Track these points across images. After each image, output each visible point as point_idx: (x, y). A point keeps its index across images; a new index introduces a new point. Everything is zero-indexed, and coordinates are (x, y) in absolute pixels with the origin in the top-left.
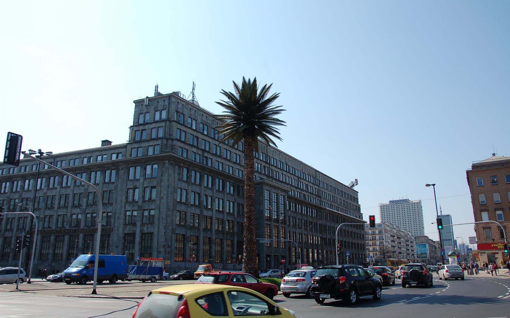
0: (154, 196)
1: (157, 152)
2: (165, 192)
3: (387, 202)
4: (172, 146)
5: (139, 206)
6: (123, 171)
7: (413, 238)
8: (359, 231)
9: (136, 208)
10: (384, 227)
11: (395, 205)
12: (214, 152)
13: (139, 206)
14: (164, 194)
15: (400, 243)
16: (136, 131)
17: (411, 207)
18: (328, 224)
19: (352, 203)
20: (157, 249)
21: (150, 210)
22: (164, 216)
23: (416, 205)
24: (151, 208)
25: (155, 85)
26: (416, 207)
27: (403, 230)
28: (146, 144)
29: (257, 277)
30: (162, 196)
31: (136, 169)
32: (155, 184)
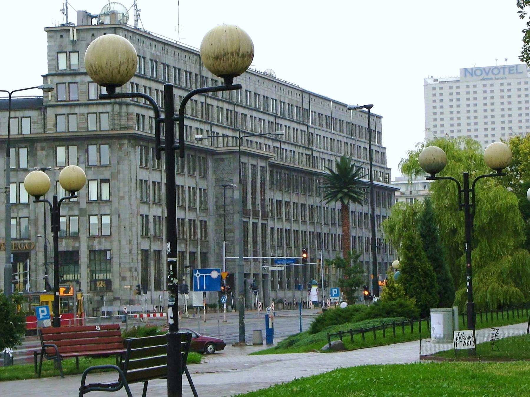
0: (105, 196)
1: (105, 125)
2: (127, 189)
3: (455, 74)
4: (128, 114)
5: (81, 210)
6: (44, 153)
8: (383, 210)
9: (77, 212)
11: (480, 84)
13: (81, 210)
14: (124, 192)
16: (57, 84)
20: (120, 273)
21: (101, 215)
22: (127, 224)
24: (102, 213)
28: (84, 110)
30: (121, 194)
31: (68, 149)
32: (106, 175)
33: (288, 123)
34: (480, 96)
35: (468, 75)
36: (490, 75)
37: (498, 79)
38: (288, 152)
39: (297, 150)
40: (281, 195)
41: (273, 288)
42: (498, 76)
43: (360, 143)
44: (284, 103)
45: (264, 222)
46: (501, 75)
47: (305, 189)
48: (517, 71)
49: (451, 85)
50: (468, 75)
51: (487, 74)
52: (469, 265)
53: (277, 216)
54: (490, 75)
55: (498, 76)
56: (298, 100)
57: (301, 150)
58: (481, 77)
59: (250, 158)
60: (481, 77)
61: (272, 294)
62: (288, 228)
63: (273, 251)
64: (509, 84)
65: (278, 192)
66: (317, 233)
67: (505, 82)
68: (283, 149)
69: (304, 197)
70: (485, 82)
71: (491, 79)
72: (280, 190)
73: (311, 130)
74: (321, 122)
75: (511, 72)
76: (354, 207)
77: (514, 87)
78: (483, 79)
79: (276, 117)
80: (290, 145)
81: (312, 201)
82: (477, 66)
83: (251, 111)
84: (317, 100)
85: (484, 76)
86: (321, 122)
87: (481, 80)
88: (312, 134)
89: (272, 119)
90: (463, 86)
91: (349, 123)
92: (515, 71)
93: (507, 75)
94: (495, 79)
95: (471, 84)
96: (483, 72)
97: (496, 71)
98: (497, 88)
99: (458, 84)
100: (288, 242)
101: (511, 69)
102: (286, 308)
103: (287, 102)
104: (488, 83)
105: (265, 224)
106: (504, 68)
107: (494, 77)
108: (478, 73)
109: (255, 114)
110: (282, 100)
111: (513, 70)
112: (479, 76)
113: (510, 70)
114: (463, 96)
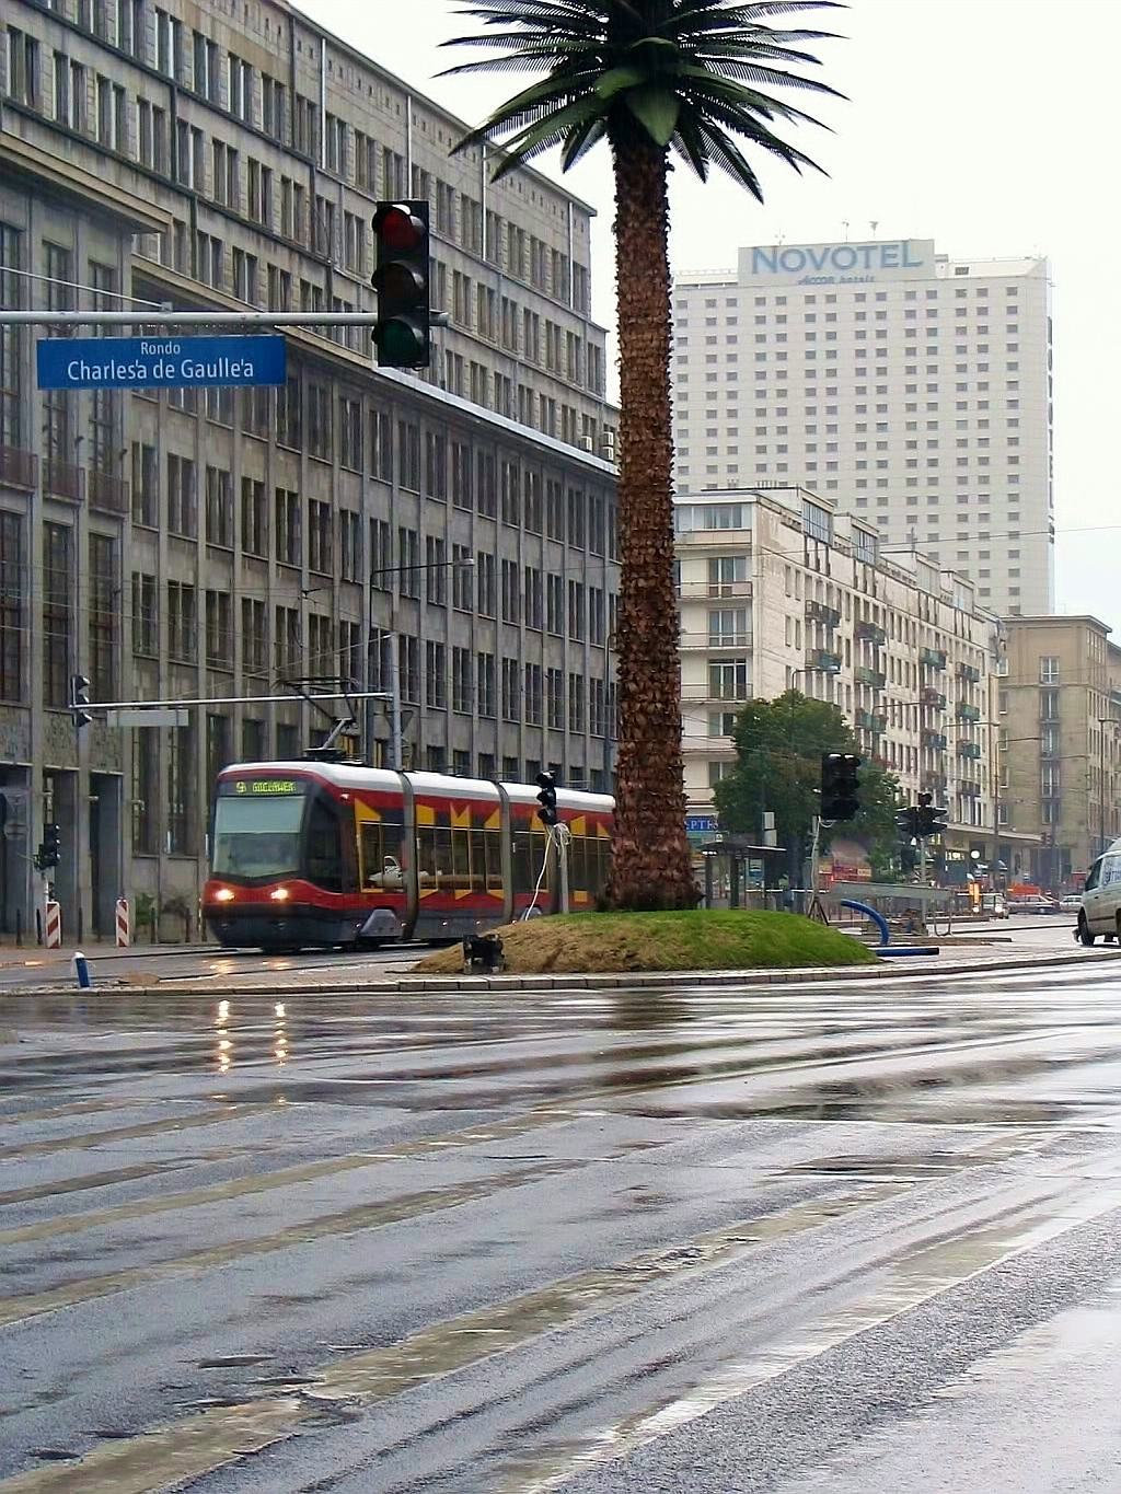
7: (981, 634)
8: (573, 560)
10: (763, 526)
11: (796, 295)
12: (288, 144)
15: (879, 681)
17: (947, 322)
18: (376, 503)
19: (545, 313)
23: (997, 302)
25: (708, 181)
26: (997, 320)
27: (906, 561)
29: (152, 899)
33: (229, 136)
34: (796, 327)
35: (761, 265)
36: (828, 270)
37: (850, 281)
38: (227, 257)
39: (267, 256)
40: (190, 437)
41: (145, 845)
42: (848, 274)
43: (514, 288)
44: (212, 45)
45: (105, 528)
46: (859, 270)
47: (296, 427)
48: (905, 256)
49: (710, 294)
50: (761, 265)
51: (818, 267)
52: (224, 1007)
53: (171, 527)
54: (828, 270)
55: (848, 274)
56: (273, 49)
57: (282, 260)
58: (801, 275)
59: (39, 210)
60: (801, 275)
61: (136, 877)
62: (220, 585)
63: (146, 683)
64: (881, 297)
65: (177, 420)
66: (343, 623)
67: (869, 289)
68: (203, 236)
69: (291, 460)
70: (810, 290)
71: (830, 280)
72: (185, 414)
73: (328, 192)
74: (365, 171)
75: (890, 261)
76: (489, 539)
77: (896, 305)
78: (806, 281)
79: (174, 89)
80: (235, 228)
81: (325, 486)
82: (788, 242)
83: (56, 31)
84: (354, 74)
85: (809, 270)
86: (365, 171)
87: (800, 283)
88: (330, 205)
89: (157, 96)
90: (746, 299)
91: (474, 204)
92: (899, 260)
93: (875, 269)
94: (843, 281)
95: (771, 295)
96: (807, 257)
97: (844, 258)
98: (846, 307)
99: (731, 294)
100: (217, 648)
101: (889, 252)
102: (196, 939)
103: (224, 42)
104: (820, 291)
105: (110, 540)
106: (867, 249)
107: (838, 275)
108: (793, 261)
109: (77, 50)
110: (206, 32)
111: (895, 256)
112: (797, 269)
113: (884, 257)
114: (746, 330)
